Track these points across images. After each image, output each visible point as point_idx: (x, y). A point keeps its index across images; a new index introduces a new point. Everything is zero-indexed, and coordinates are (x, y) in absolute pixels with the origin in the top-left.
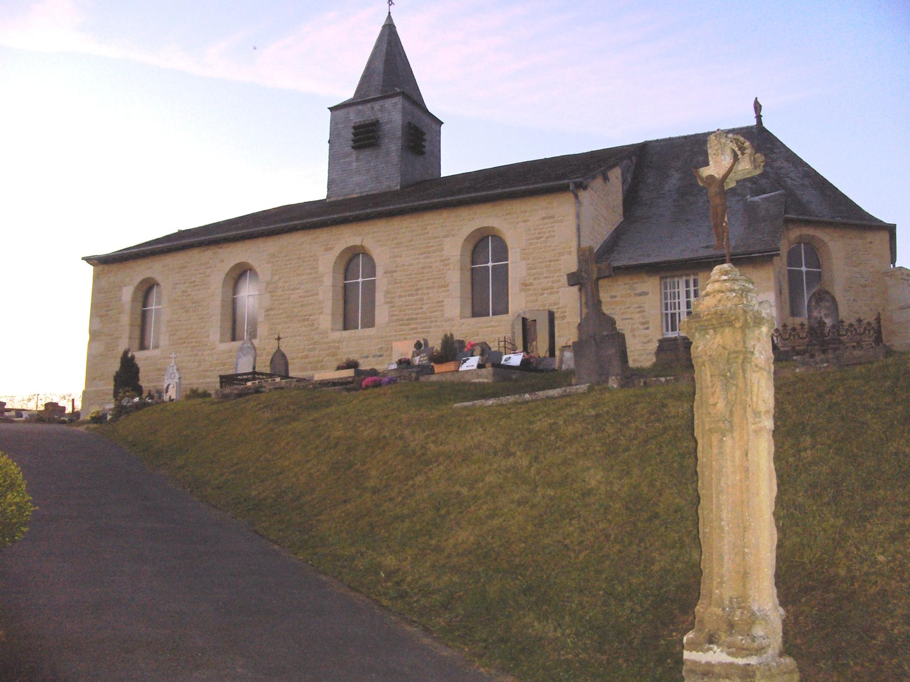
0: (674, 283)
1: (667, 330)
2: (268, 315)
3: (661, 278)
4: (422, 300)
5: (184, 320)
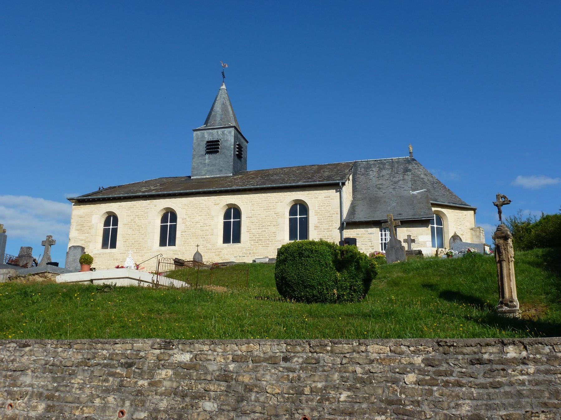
2: (182, 234)
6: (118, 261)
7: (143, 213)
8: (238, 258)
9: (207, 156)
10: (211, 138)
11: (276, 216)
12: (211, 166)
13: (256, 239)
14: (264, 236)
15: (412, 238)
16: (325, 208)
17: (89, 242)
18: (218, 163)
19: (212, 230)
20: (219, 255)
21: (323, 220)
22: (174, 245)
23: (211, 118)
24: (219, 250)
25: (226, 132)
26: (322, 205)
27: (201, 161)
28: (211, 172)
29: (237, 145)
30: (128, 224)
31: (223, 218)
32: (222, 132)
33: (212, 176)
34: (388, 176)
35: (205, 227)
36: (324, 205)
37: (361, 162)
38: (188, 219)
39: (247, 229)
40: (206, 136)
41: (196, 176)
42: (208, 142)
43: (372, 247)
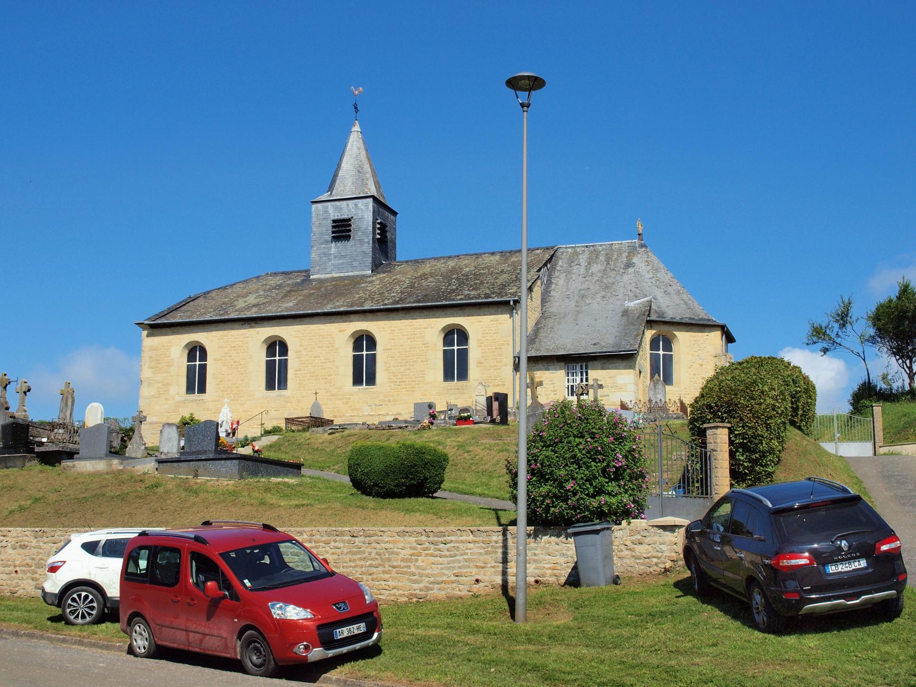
0: (573, 366)
1: (568, 395)
2: (296, 374)
3: (566, 364)
4: (409, 369)
5: (410, 362)
6: (209, 412)
7: (241, 343)
8: (374, 406)
9: (333, 245)
10: (339, 214)
11: (424, 348)
12: (339, 259)
13: (398, 380)
14: (408, 377)
15: (599, 383)
16: (491, 336)
17: (168, 385)
18: (350, 254)
19: (337, 367)
20: (347, 403)
21: (488, 354)
22: (285, 388)
23: (338, 182)
24: (348, 396)
25: (360, 205)
26: (487, 331)
27: (324, 251)
28: (339, 268)
29: (379, 223)
30: (221, 360)
31: (351, 349)
32: (355, 205)
33: (342, 275)
34: (600, 275)
35: (328, 364)
36: (490, 331)
37: (566, 248)
38: (304, 353)
39: (385, 366)
40: (331, 212)
41: (317, 273)
42: (334, 221)
43: (555, 391)
